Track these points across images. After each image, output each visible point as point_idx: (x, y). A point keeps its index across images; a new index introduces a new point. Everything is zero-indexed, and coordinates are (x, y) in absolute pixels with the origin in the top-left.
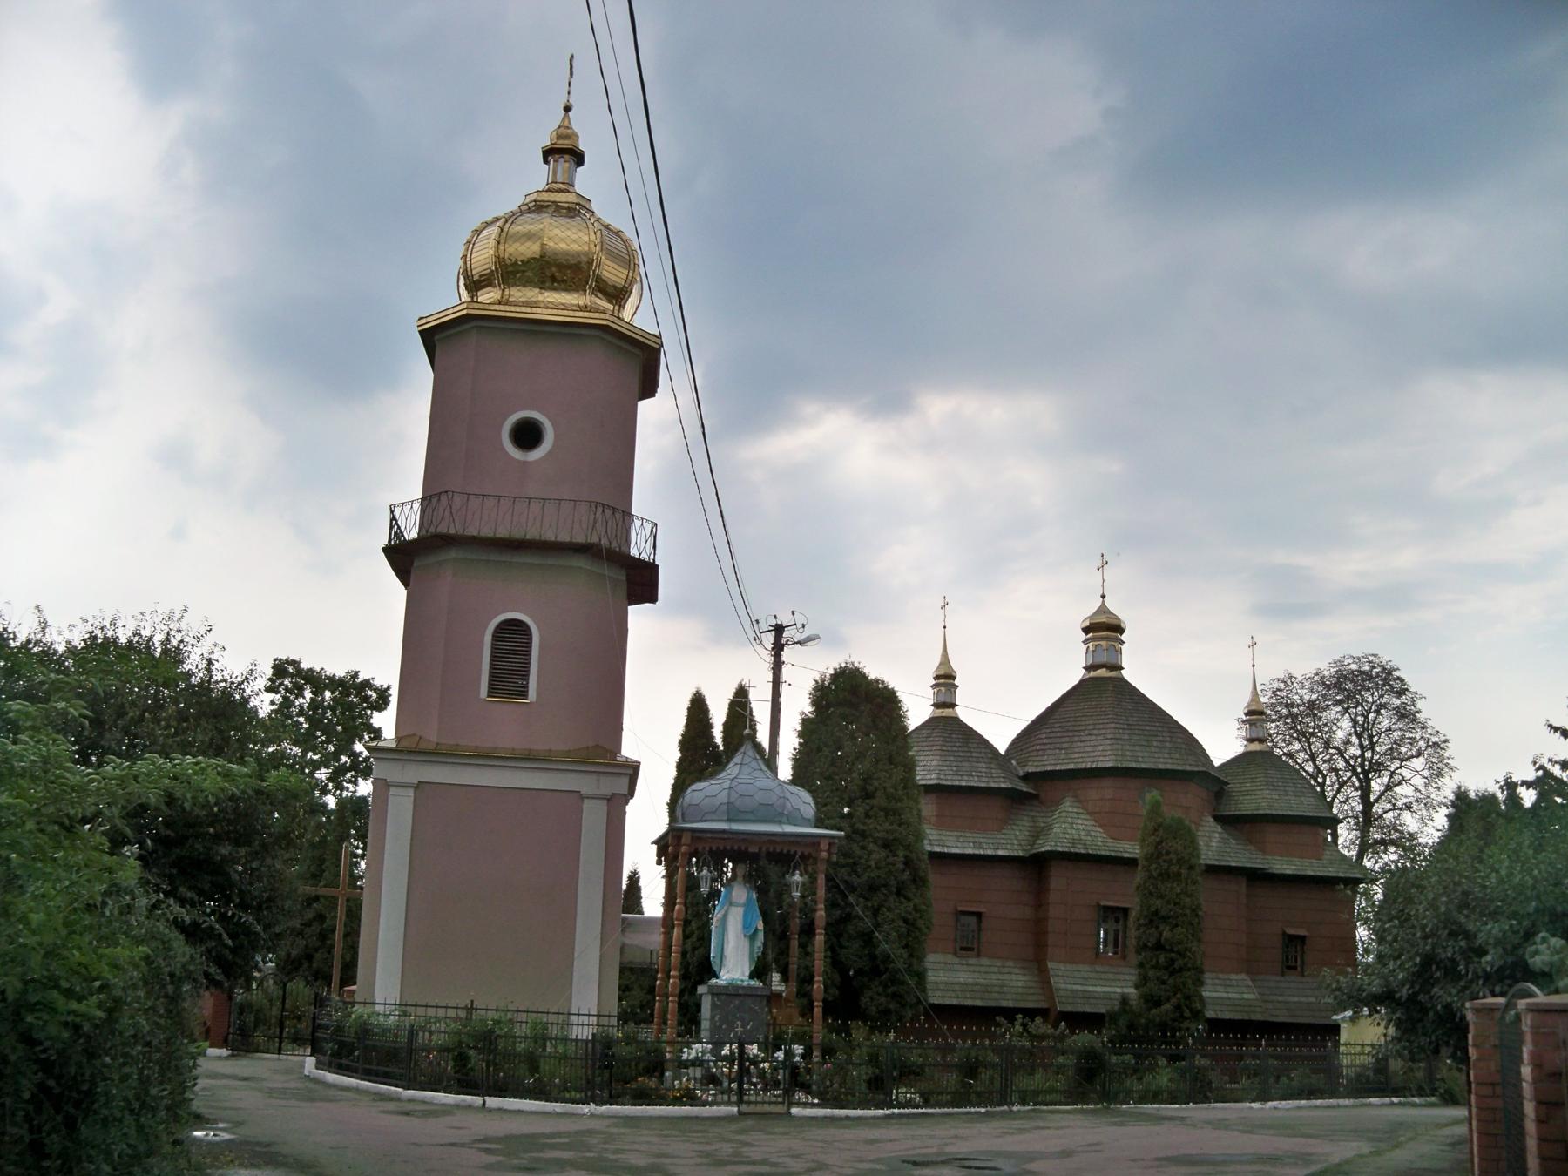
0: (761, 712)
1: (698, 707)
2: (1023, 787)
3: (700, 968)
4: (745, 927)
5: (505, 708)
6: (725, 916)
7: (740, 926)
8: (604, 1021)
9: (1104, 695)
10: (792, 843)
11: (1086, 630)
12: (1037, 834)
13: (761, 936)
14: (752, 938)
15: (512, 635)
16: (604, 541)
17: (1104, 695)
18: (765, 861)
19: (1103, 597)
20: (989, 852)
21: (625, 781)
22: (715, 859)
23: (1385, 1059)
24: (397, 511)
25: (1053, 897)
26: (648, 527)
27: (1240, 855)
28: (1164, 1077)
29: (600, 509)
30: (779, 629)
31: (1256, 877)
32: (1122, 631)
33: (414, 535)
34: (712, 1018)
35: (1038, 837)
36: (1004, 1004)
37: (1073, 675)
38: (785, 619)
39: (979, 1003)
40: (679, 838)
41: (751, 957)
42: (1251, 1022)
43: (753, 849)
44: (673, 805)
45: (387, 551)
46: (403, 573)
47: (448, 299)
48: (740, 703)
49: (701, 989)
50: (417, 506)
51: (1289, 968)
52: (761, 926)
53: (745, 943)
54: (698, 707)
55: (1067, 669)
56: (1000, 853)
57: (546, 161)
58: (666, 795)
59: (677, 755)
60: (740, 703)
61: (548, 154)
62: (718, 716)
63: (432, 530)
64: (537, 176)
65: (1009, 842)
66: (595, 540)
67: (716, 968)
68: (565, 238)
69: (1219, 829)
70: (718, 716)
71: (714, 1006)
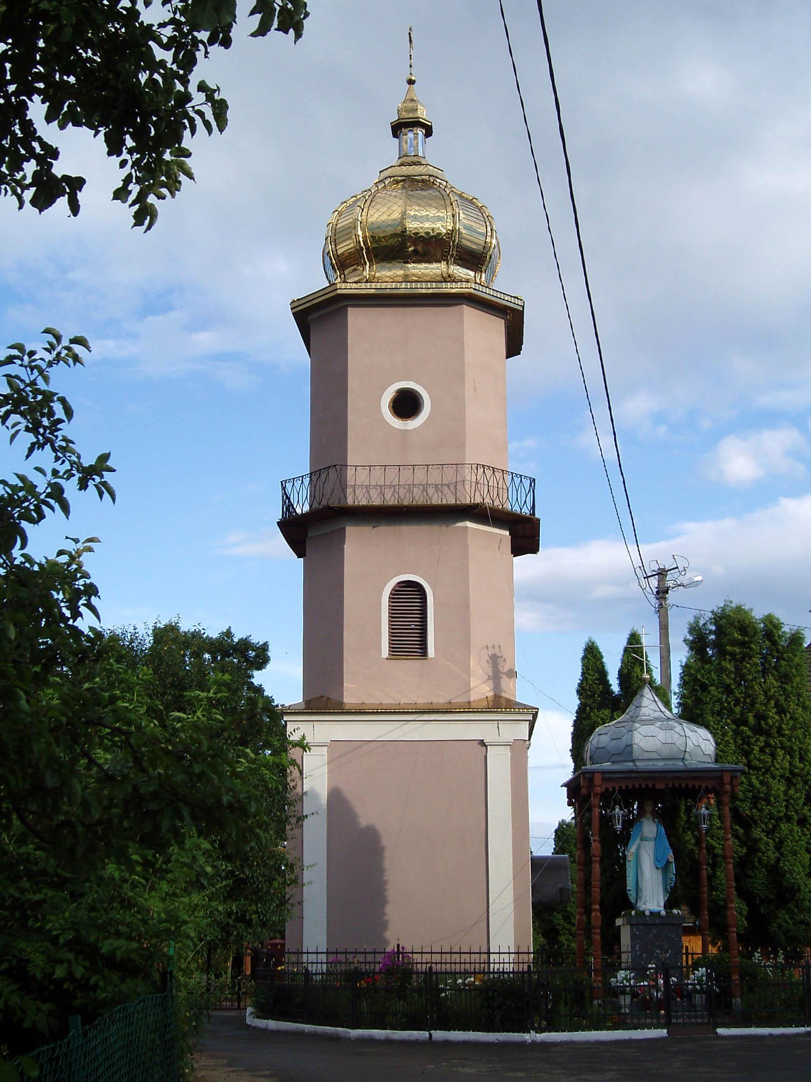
0: (654, 660)
1: (592, 657)
3: (618, 898)
4: (656, 860)
5: (408, 667)
6: (638, 850)
8: (525, 957)
10: (675, 778)
13: (673, 866)
14: (665, 869)
15: (410, 596)
16: (488, 501)
18: (667, 792)
21: (526, 725)
22: (627, 797)
24: (289, 486)
26: (527, 483)
29: (481, 470)
33: (306, 508)
34: (633, 947)
40: (591, 780)
41: (665, 890)
43: (660, 786)
44: (577, 753)
45: (284, 525)
46: (298, 545)
47: (314, 280)
48: (634, 643)
49: (619, 922)
50: (307, 481)
52: (671, 856)
53: (659, 875)
54: (592, 657)
57: (395, 135)
58: (567, 744)
59: (572, 729)
60: (634, 648)
61: (398, 129)
62: (613, 666)
63: (324, 503)
64: (387, 152)
66: (478, 500)
67: (633, 901)
68: (428, 219)
70: (613, 666)
71: (633, 936)
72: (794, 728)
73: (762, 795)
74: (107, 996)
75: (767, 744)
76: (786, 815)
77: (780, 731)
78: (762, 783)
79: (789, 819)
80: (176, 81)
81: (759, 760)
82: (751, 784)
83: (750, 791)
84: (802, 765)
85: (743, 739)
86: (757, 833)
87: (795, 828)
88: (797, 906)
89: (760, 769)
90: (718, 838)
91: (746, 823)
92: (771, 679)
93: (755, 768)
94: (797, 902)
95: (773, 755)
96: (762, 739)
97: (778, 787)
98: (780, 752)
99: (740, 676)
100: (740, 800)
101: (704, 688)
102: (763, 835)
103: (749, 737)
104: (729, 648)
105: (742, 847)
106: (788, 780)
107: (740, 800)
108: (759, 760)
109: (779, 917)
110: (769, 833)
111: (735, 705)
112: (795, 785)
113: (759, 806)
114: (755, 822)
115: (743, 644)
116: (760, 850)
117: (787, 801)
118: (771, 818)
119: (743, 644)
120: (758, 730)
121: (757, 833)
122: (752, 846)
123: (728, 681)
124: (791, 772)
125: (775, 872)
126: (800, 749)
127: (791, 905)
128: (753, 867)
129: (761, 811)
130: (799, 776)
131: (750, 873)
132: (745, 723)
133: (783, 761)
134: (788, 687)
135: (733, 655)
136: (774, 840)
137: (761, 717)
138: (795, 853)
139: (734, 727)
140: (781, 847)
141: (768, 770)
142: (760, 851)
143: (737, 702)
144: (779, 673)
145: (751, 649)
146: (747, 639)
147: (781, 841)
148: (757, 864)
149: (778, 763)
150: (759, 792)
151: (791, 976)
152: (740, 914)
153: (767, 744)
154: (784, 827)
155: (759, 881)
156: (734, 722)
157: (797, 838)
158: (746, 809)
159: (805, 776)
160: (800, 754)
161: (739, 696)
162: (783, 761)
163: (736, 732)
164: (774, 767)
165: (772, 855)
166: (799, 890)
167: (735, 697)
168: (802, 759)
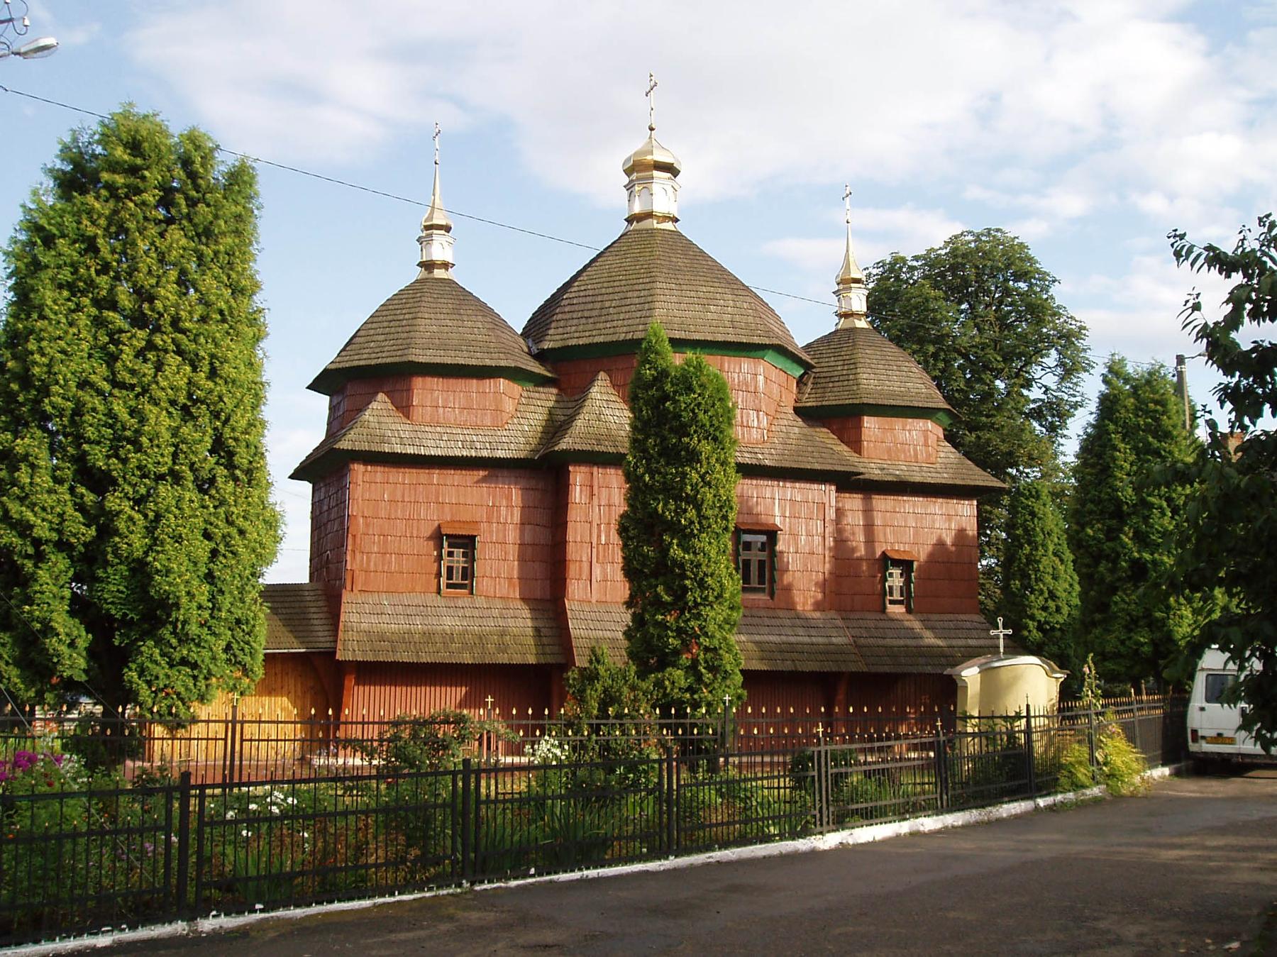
11: (628, 172)
20: (485, 454)
69: (801, 423)
72: (203, 319)
73: (128, 433)
74: (18, 677)
75: (151, 346)
76: (171, 471)
77: (175, 322)
78: (133, 412)
79: (177, 478)
80: (1267, 406)
81: (133, 372)
82: (110, 413)
83: (111, 427)
84: (211, 384)
85: (110, 335)
86: (113, 502)
87: (187, 495)
88: (174, 633)
89: (132, 387)
90: (44, 509)
91: (101, 482)
92: (174, 233)
93: (122, 386)
94: (175, 627)
95: (159, 367)
96: (142, 334)
97: (161, 421)
98: (173, 360)
99: (117, 229)
100: (89, 442)
101: (49, 241)
102: (126, 506)
103: (121, 331)
104: (105, 176)
105: (88, 526)
106: (185, 408)
107: (89, 442)
108: (133, 372)
109: (141, 653)
110: (139, 502)
111: (98, 273)
112: (195, 418)
113: (122, 452)
114: (114, 482)
115: (133, 171)
116: (116, 532)
117: (176, 446)
118: (144, 476)
119: (133, 171)
120: (138, 320)
121: (113, 502)
122: (105, 524)
123: (91, 231)
124: (190, 396)
125: (140, 571)
126: (212, 356)
127: (166, 632)
128: (106, 563)
129: (125, 461)
130: (203, 402)
131: (100, 573)
132: (114, 306)
133: (176, 374)
134: (208, 252)
135: (110, 187)
136: (146, 516)
137: (144, 295)
138: (178, 539)
139: (94, 311)
140: (156, 528)
141: (145, 391)
142: (120, 535)
143: (105, 269)
144: (195, 225)
145: (143, 178)
146: (139, 161)
147: (158, 517)
148: (110, 557)
149: (167, 378)
150: (124, 429)
151: (574, 679)
152: (72, 645)
153: (151, 346)
154: (165, 491)
155: (113, 586)
156: (96, 303)
157: (188, 512)
158: (98, 457)
159: (215, 404)
160: (211, 364)
161: (109, 257)
162: (176, 374)
163: (98, 322)
164: (157, 383)
165: (138, 542)
166: (177, 606)
167: (103, 259)
168: (213, 374)
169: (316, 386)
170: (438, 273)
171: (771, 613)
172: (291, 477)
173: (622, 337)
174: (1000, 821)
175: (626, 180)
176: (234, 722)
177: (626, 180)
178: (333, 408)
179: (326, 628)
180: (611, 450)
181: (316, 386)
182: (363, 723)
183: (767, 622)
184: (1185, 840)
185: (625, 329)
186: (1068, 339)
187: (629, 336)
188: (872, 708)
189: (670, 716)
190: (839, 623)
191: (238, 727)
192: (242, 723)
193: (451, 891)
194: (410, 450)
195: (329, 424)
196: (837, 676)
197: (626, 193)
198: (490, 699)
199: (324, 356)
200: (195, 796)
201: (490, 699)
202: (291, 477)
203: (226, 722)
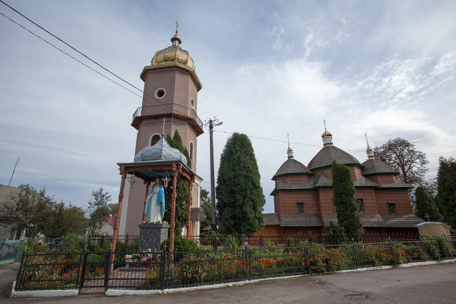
2: (310, 172)
6: (151, 197)
7: (156, 201)
9: (328, 148)
11: (323, 137)
12: (316, 182)
17: (328, 148)
19: (326, 129)
20: (303, 188)
23: (65, 237)
25: (321, 197)
27: (369, 184)
28: (147, 303)
30: (211, 121)
31: (377, 189)
32: (331, 136)
35: (315, 184)
36: (311, 225)
37: (321, 147)
38: (213, 119)
39: (304, 226)
42: (382, 228)
51: (391, 212)
55: (320, 145)
56: (306, 188)
65: (308, 184)
69: (364, 178)
169: (273, 179)
170: (291, 158)
171: (364, 215)
172: (270, 195)
173: (326, 165)
174: (445, 264)
175: (322, 138)
176: (261, 237)
177: (322, 138)
178: (276, 183)
179: (278, 220)
180: (327, 185)
181: (273, 179)
182: (256, 237)
183: (364, 217)
184: (138, 165)
185: (326, 164)
186: (421, 156)
187: (327, 165)
188: (373, 234)
189: (349, 235)
190: (380, 217)
191: (262, 238)
192: (262, 237)
193: (289, 277)
194: (290, 188)
195: (275, 185)
196: (382, 228)
197: (323, 141)
198: (310, 232)
199: (274, 173)
200: (71, 276)
201: (310, 232)
202: (270, 195)
203: (259, 237)
